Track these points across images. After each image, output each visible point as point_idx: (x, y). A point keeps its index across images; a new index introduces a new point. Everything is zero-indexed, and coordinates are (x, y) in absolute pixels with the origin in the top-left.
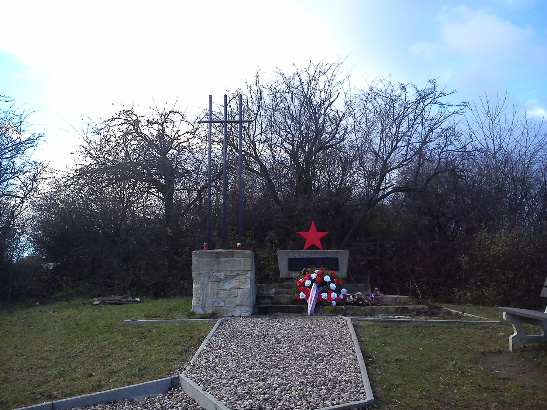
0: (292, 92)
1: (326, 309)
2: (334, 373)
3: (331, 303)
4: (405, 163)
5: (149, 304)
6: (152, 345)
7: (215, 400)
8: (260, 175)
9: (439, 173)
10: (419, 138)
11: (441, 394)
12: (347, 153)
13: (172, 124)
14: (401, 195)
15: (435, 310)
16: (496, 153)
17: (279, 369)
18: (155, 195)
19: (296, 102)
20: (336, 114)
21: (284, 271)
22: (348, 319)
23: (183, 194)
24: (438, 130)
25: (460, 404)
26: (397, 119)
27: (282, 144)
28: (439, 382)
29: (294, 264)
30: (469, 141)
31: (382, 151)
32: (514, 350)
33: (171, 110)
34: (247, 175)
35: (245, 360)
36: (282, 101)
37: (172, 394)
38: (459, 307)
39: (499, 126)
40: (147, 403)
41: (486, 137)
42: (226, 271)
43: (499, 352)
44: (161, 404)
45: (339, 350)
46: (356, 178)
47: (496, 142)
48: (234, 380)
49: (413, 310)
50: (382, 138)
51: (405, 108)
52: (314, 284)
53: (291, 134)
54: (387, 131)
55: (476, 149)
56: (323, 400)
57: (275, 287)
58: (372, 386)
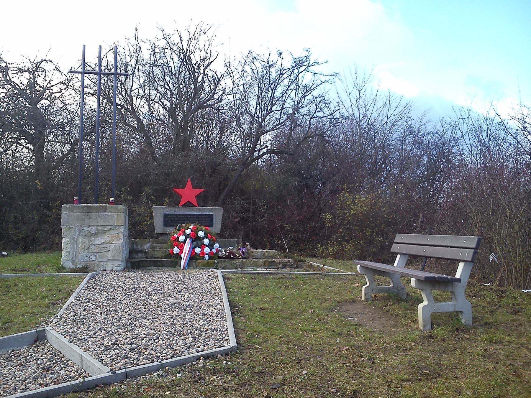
0: (172, 50)
2: (202, 322)
3: (204, 257)
4: (279, 126)
5: (17, 258)
6: (18, 298)
7: (81, 351)
8: (136, 130)
9: (309, 138)
10: (292, 103)
11: (299, 339)
12: (224, 114)
13: (44, 73)
14: (274, 157)
15: (299, 263)
16: (360, 121)
17: (148, 320)
18: (24, 146)
19: (176, 59)
20: (215, 75)
21: (159, 227)
22: (219, 272)
23: (55, 147)
24: (310, 97)
25: (315, 348)
26: (272, 84)
27: (160, 100)
28: (298, 328)
29: (169, 220)
30: (337, 108)
31: (258, 113)
32: (367, 300)
33: (44, 59)
34: (124, 130)
35: (114, 313)
36: (161, 58)
37: (37, 346)
38: (321, 261)
39: (364, 96)
40: (11, 356)
41: (353, 106)
42: (98, 226)
43: (353, 301)
44: (26, 357)
45: (208, 301)
46: (233, 139)
47: (361, 111)
48: (101, 331)
49: (280, 263)
50: (258, 101)
51: (281, 73)
52: (188, 239)
53: (170, 90)
54: (263, 94)
55: (342, 116)
56: (189, 348)
57: (149, 242)
58: (236, 334)
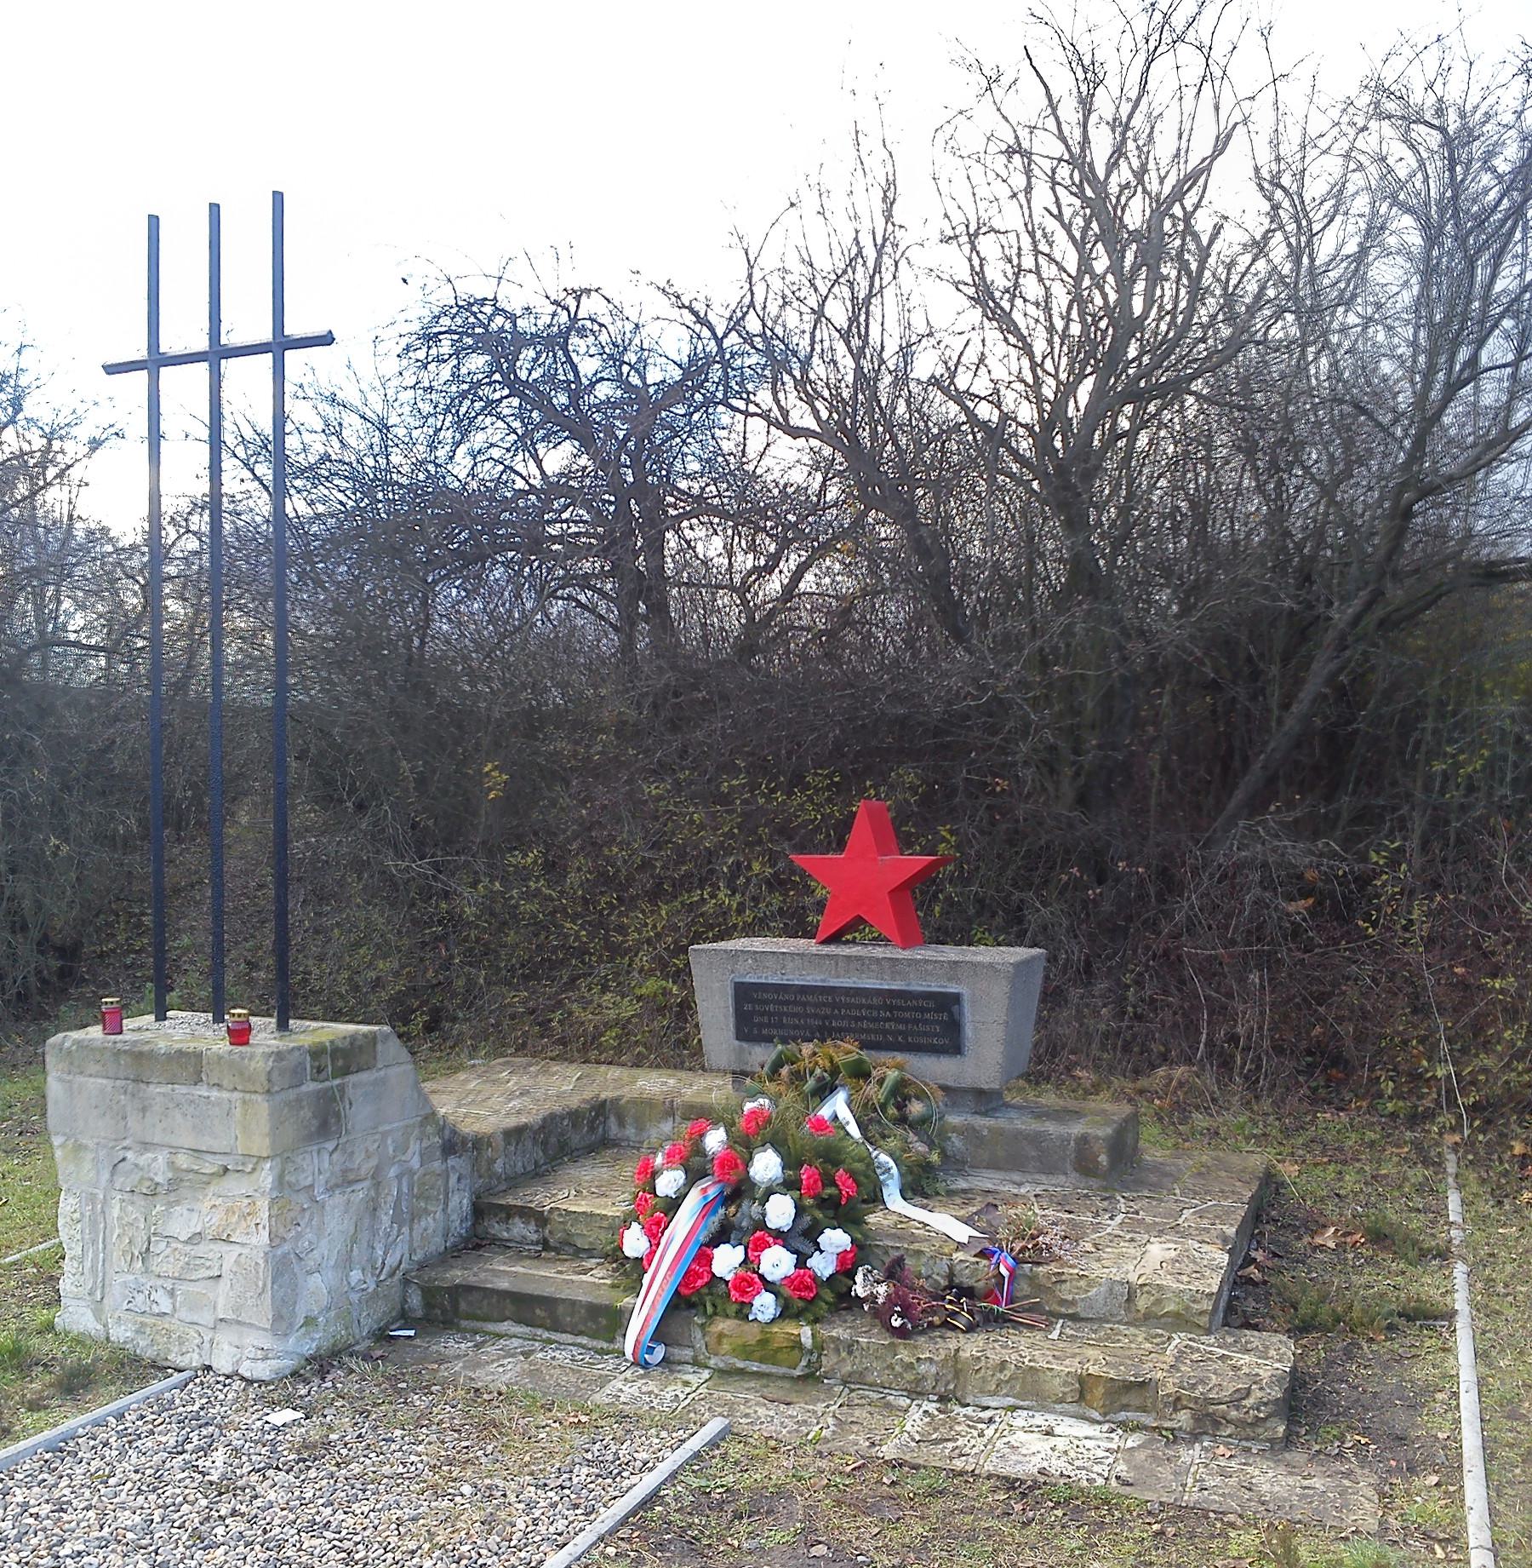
1: (721, 1336)
42: (174, 1150)
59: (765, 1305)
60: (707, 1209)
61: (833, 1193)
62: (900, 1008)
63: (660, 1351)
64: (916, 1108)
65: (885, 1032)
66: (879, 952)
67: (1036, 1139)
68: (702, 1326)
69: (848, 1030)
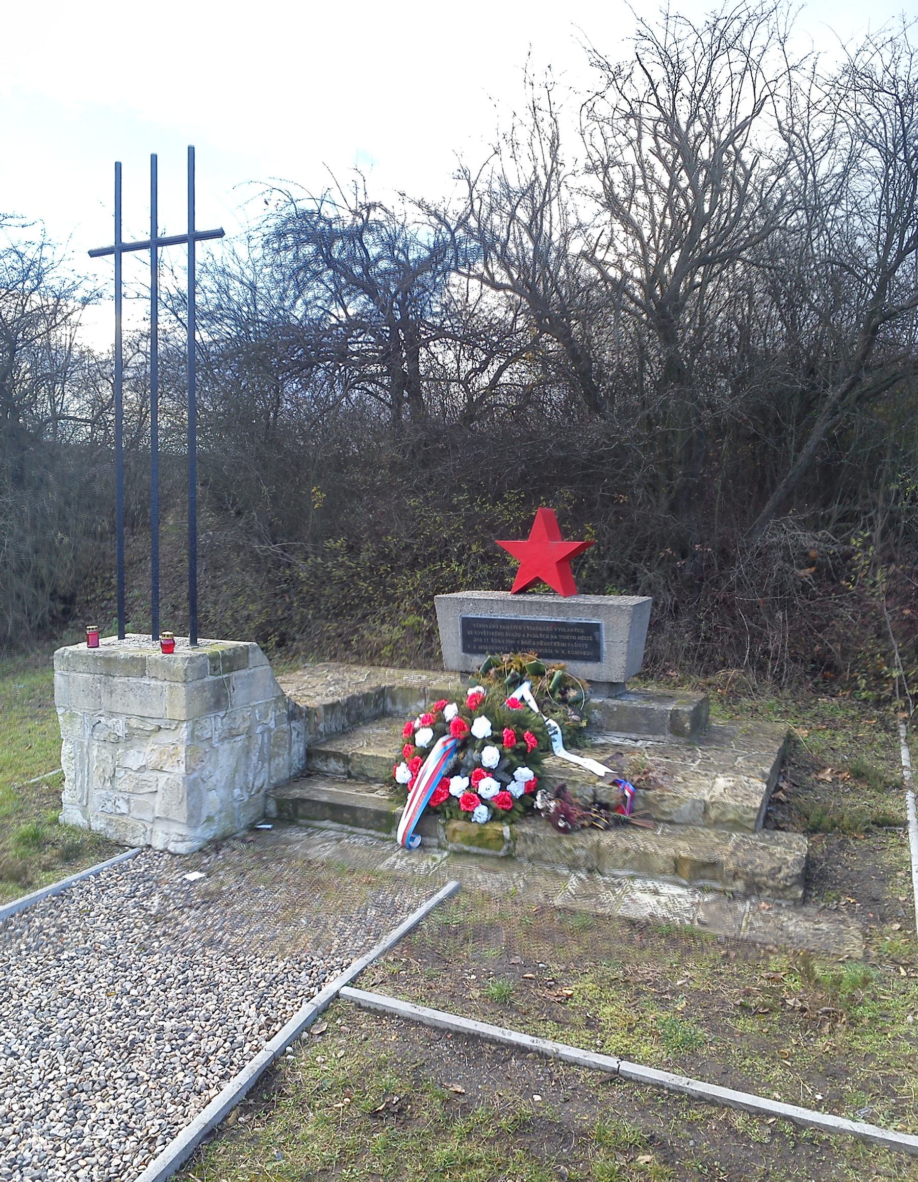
1: (455, 831)
42: (129, 716)
59: (481, 813)
60: (446, 755)
61: (522, 744)
62: (563, 633)
63: (418, 840)
64: (572, 694)
65: (554, 648)
66: (549, 599)
67: (646, 712)
68: (444, 825)
69: (532, 647)
